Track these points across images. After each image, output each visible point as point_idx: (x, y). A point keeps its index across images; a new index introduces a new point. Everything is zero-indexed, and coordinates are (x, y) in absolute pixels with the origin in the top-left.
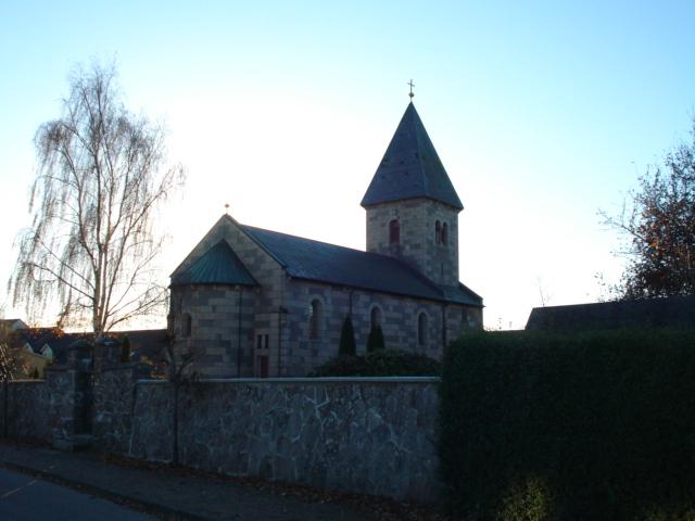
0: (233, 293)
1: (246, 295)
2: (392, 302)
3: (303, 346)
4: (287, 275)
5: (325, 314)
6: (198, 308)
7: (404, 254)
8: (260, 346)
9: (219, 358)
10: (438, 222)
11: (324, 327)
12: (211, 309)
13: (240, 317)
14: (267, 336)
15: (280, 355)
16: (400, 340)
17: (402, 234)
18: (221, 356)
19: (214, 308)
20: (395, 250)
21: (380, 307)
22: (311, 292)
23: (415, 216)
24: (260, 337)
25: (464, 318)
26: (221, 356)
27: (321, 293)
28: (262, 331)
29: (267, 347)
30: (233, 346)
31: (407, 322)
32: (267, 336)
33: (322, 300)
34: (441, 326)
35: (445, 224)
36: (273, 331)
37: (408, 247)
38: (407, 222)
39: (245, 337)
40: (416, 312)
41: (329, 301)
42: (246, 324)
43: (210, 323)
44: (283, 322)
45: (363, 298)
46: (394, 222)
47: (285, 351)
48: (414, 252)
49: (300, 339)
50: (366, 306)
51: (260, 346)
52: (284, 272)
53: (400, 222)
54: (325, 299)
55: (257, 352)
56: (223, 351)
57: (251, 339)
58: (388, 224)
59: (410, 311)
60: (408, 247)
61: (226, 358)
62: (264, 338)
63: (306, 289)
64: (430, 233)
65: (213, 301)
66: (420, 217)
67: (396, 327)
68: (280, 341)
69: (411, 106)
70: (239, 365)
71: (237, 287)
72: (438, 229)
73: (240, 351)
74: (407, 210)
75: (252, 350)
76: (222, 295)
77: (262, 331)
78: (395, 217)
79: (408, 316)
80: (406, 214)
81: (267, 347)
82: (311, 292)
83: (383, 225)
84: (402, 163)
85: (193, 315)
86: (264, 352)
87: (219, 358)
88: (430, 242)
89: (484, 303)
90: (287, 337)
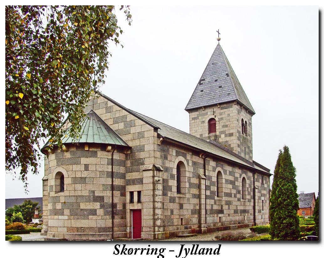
0: (105, 153)
1: (117, 156)
2: (229, 168)
3: (172, 200)
4: (159, 136)
5: (188, 174)
6: (71, 167)
7: (220, 141)
8: (132, 201)
9: (93, 212)
10: (242, 120)
11: (187, 185)
12: (83, 168)
13: (112, 175)
14: (139, 193)
15: (154, 208)
16: (233, 196)
17: (218, 127)
18: (95, 210)
19: (87, 167)
20: (213, 138)
21: (222, 172)
22: (178, 154)
23: (229, 115)
24: (132, 193)
25: (262, 183)
26: (95, 210)
27: (185, 156)
28: (134, 188)
29: (139, 201)
30: (106, 201)
31: (237, 184)
32: (139, 193)
33: (185, 163)
34: (253, 187)
35: (246, 121)
36: (147, 189)
37: (223, 136)
38: (222, 119)
39: (117, 193)
40: (241, 175)
41: (190, 164)
42: (118, 182)
43: (83, 180)
44: (156, 179)
45: (212, 163)
46: (211, 120)
47: (158, 205)
48: (228, 139)
49: (169, 195)
50: (214, 170)
51: (132, 201)
52: (156, 134)
53: (217, 119)
54: (188, 161)
55: (129, 207)
56: (97, 205)
57: (123, 194)
58: (207, 121)
59: (237, 175)
60: (223, 136)
61: (100, 212)
62: (136, 195)
63: (173, 151)
64: (236, 127)
65: (84, 161)
66: (230, 118)
67: (230, 186)
68: (154, 195)
69: (219, 47)
70: (113, 218)
71: (110, 148)
72: (243, 124)
73: (113, 206)
74: (222, 111)
75: (124, 205)
76: (95, 155)
77: (134, 188)
78: (213, 117)
79: (236, 179)
80: (221, 114)
81: (139, 201)
82: (178, 154)
83: (203, 122)
84: (216, 81)
85: (65, 175)
86: (136, 206)
87: (93, 212)
88: (238, 132)
89: (296, 173)
90: (160, 193)
